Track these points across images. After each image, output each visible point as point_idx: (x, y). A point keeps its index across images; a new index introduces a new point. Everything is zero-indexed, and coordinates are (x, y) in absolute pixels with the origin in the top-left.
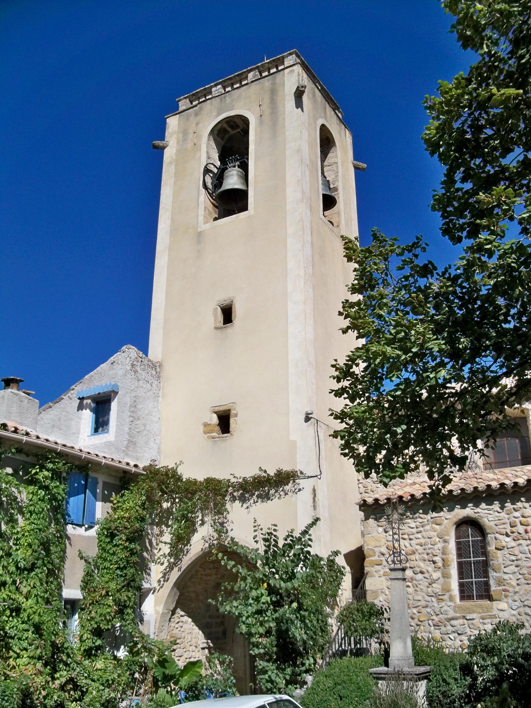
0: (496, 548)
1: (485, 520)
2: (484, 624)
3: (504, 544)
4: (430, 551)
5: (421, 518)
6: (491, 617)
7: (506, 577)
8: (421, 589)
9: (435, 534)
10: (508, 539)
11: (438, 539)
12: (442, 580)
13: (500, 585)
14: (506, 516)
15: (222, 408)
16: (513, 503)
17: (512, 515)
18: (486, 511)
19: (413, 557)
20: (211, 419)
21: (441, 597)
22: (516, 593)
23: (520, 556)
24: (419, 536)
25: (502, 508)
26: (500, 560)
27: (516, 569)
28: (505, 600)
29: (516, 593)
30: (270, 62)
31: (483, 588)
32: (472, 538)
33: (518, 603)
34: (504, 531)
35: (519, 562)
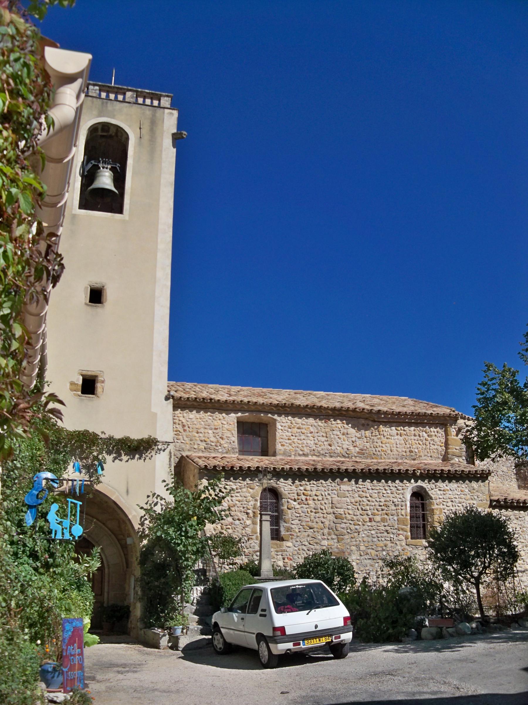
0: (288, 508)
1: (282, 489)
2: (277, 555)
3: (293, 506)
4: (245, 506)
5: (240, 483)
6: (282, 551)
7: (293, 526)
8: (238, 531)
9: (249, 495)
10: (295, 503)
11: (251, 499)
12: (252, 526)
13: (288, 531)
14: (296, 489)
15: (90, 373)
16: (299, 481)
17: (298, 488)
18: (283, 484)
19: (233, 509)
20: (78, 380)
21: (251, 537)
22: (297, 536)
23: (302, 514)
24: (238, 495)
25: (293, 483)
26: (290, 516)
27: (299, 522)
28: (291, 541)
29: (297, 536)
30: (149, 93)
31: (275, 533)
32: (270, 500)
33: (299, 543)
34: (293, 498)
35: (301, 518)
